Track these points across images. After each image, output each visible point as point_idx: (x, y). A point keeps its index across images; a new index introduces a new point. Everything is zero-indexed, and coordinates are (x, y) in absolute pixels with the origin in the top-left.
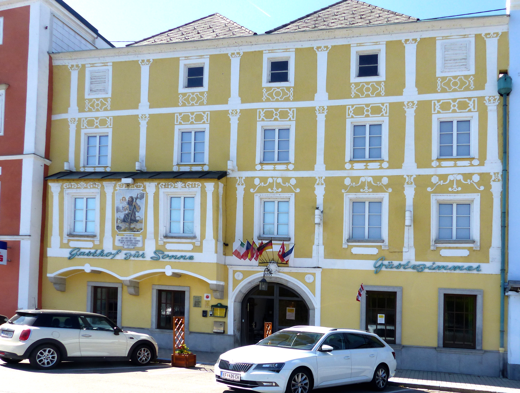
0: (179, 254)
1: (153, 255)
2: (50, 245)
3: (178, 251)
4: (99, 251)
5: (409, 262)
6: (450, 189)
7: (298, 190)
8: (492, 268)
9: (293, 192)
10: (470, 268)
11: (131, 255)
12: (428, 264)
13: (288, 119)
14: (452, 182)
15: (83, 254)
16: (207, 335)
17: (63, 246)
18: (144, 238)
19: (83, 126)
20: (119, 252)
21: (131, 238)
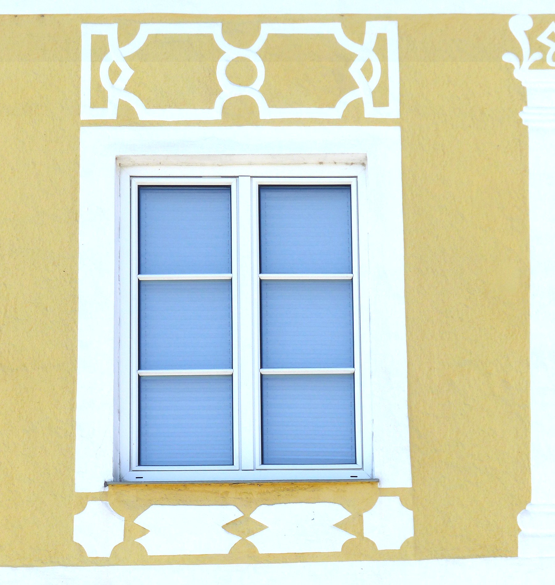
19: (99, 98)
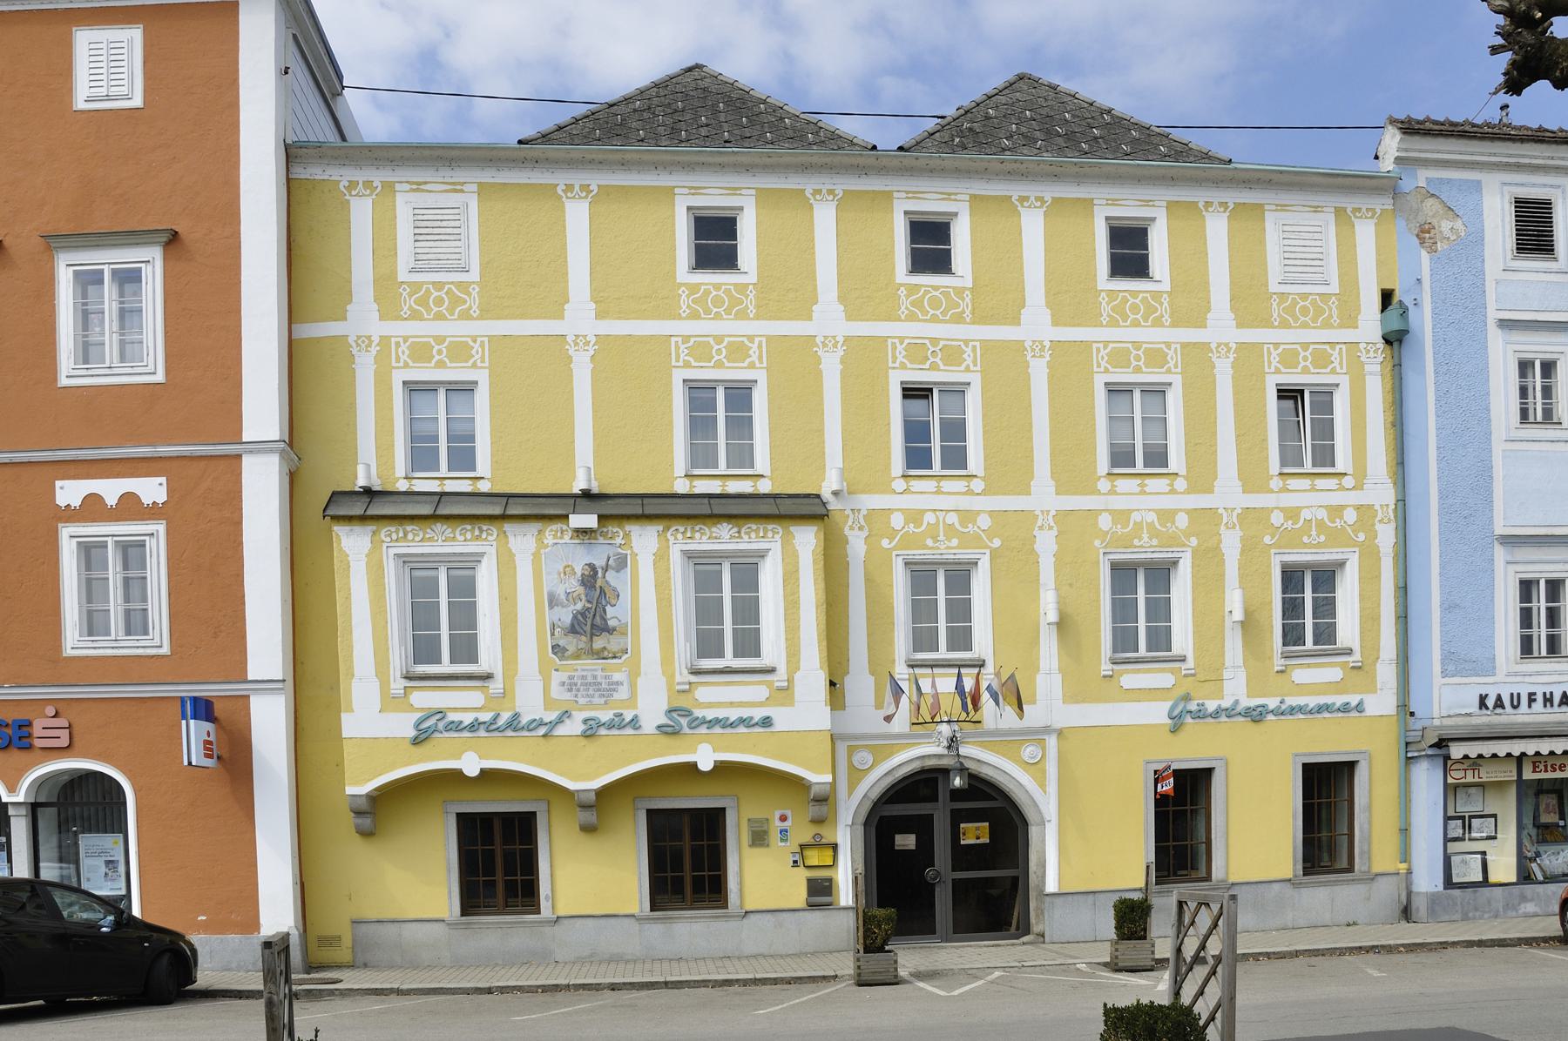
0: (733, 714)
1: (664, 720)
2: (350, 702)
3: (732, 704)
4: (505, 716)
5: (1237, 702)
6: (1305, 539)
7: (997, 543)
8: (1382, 703)
9: (987, 547)
10: (1345, 708)
11: (600, 725)
12: (1272, 703)
13: (963, 368)
14: (1139, 525)
15: (456, 727)
16: (769, 916)
17: (391, 703)
18: (634, 673)
19: (1099, 366)
20: (566, 714)
21: (595, 677)
